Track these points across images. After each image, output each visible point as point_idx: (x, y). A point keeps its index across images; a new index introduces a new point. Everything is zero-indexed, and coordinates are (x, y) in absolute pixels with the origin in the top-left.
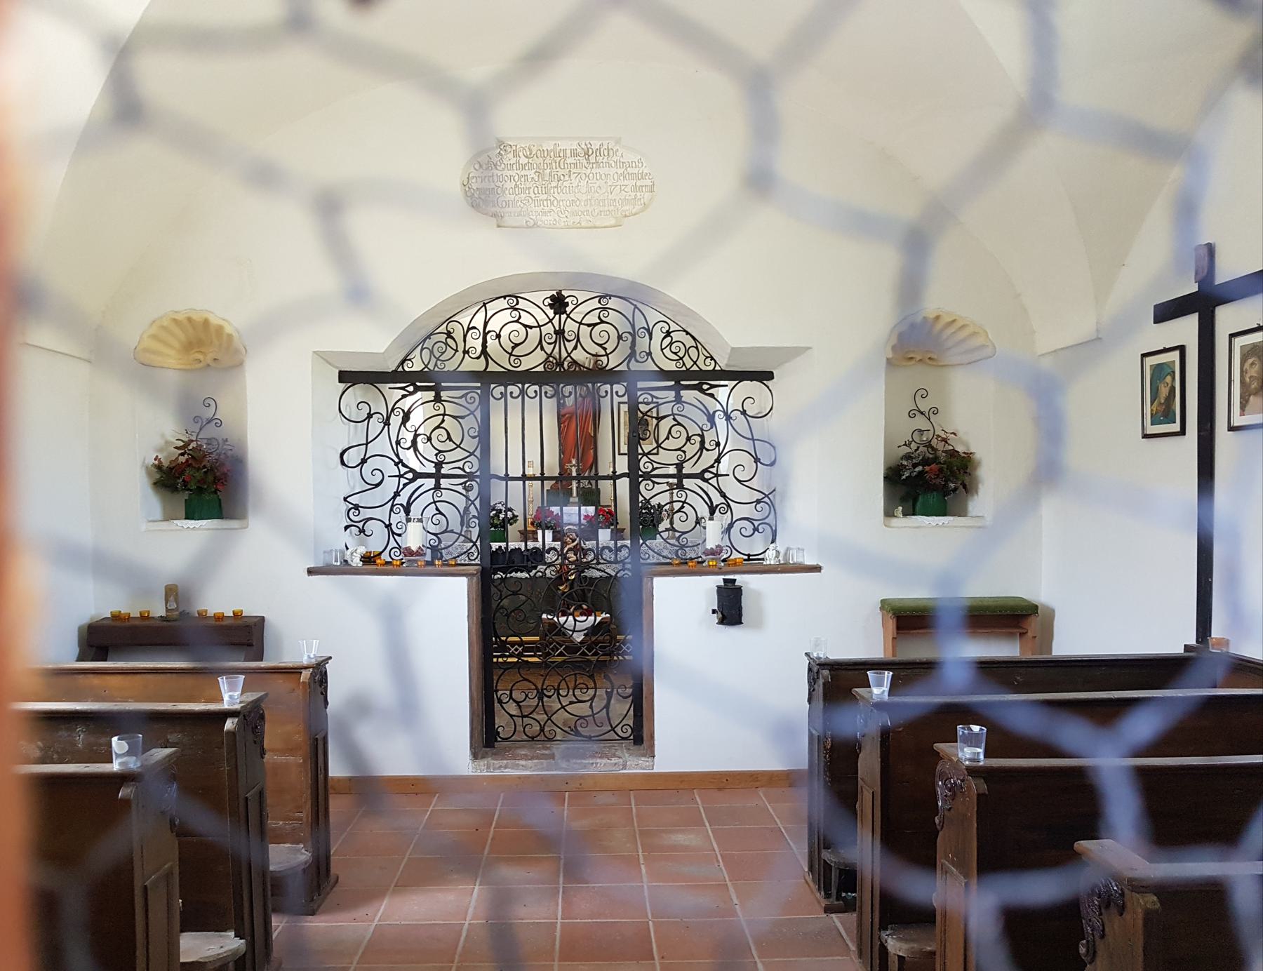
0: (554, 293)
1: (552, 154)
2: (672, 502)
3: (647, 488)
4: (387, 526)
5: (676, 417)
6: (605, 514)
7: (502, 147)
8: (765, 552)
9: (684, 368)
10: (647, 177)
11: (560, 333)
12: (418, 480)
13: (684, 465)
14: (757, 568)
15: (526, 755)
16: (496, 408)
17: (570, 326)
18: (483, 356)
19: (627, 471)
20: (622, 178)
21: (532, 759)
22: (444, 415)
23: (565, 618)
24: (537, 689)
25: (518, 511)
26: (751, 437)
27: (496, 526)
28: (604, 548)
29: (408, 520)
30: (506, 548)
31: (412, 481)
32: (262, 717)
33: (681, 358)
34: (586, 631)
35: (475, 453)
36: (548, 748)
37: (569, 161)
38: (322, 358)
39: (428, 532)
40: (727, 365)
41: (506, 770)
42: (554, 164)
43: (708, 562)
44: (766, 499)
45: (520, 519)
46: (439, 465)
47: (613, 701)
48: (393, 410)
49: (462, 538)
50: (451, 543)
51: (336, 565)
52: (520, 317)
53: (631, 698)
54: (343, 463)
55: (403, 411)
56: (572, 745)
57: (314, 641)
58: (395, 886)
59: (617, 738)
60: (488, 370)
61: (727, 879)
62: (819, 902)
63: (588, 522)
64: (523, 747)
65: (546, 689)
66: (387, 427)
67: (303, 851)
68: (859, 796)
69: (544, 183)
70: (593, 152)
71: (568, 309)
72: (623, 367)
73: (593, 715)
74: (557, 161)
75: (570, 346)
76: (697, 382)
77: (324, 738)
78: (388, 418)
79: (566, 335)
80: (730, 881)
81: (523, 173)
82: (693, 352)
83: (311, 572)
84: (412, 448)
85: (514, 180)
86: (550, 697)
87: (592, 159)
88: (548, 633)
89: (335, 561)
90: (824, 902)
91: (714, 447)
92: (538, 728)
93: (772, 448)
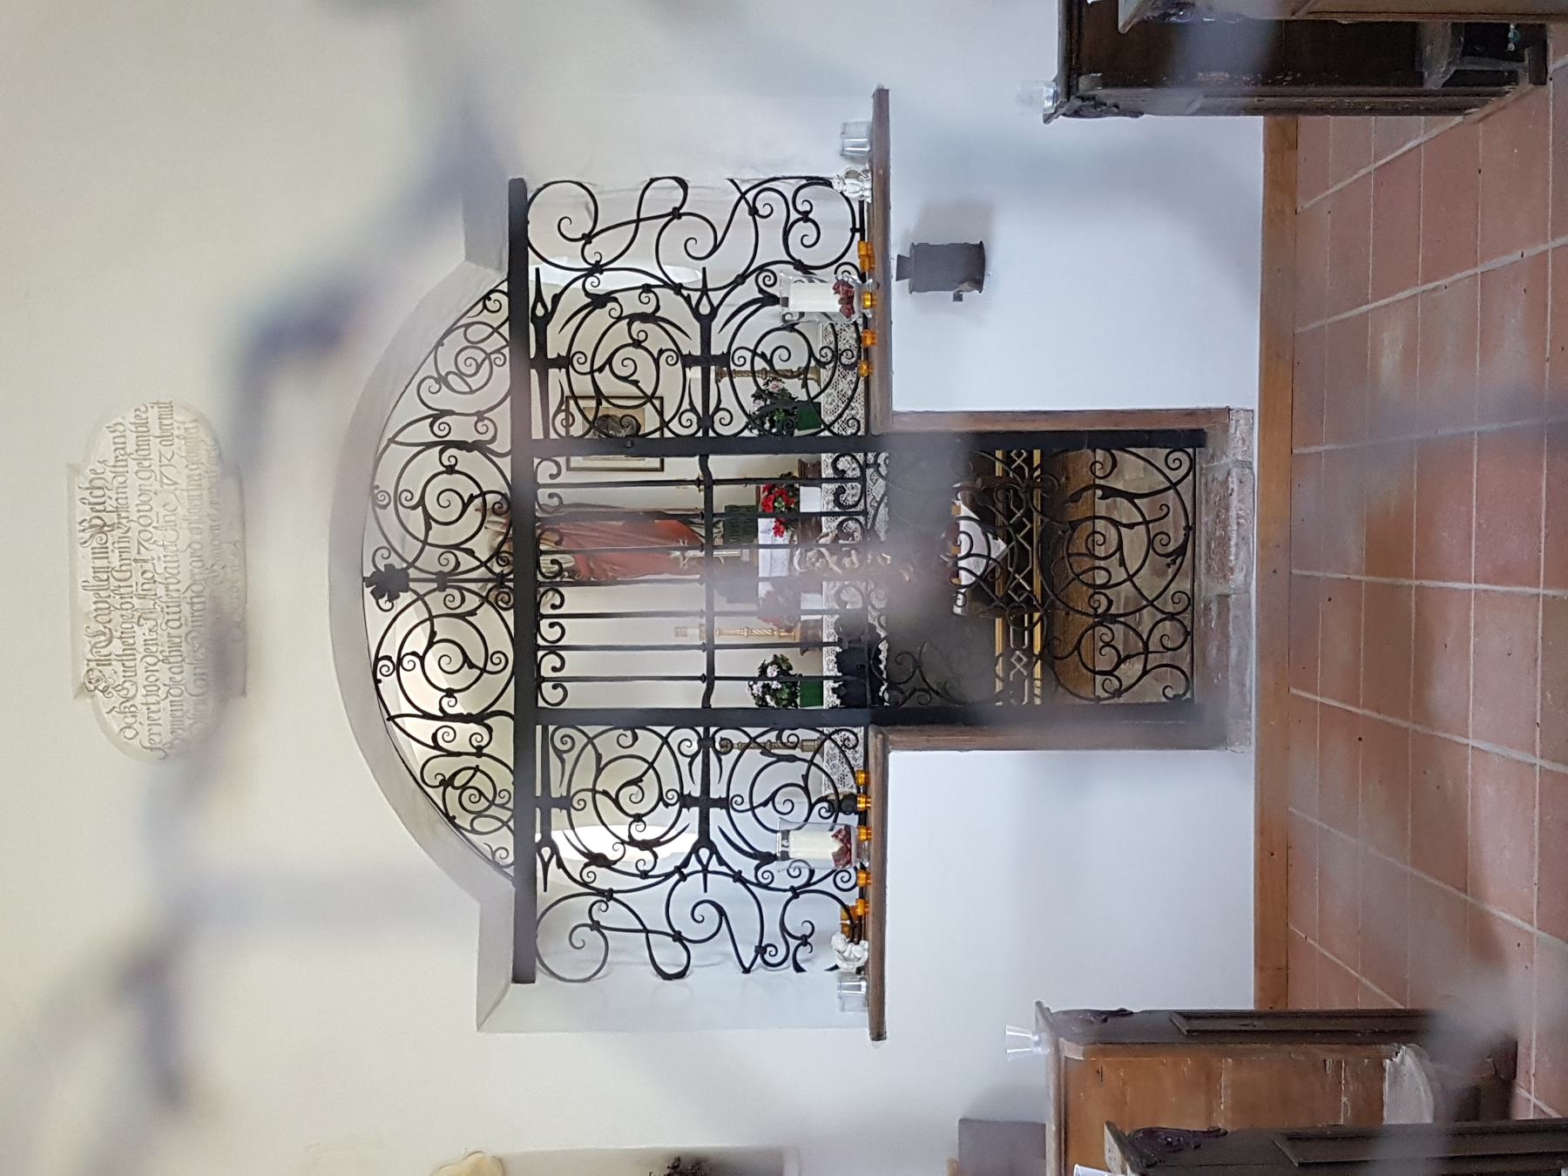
0: (368, 591)
1: (103, 594)
2: (753, 373)
3: (727, 421)
4: (796, 896)
5: (595, 367)
6: (772, 497)
7: (92, 687)
8: (847, 199)
9: (506, 351)
10: (144, 416)
11: (443, 581)
12: (712, 838)
13: (685, 352)
14: (877, 213)
15: (1219, 649)
16: (580, 697)
17: (431, 561)
18: (487, 722)
19: (697, 458)
20: (146, 463)
21: (1225, 635)
22: (594, 791)
23: (962, 573)
24: (1092, 627)
25: (768, 656)
26: (634, 225)
27: (793, 695)
28: (837, 502)
29: (785, 856)
30: (835, 679)
31: (714, 850)
32: (1151, 1133)
33: (488, 356)
34: (990, 536)
35: (664, 735)
36: (1207, 608)
37: (116, 563)
38: (490, 1013)
39: (806, 820)
40: (499, 269)
41: (1248, 683)
42: (122, 590)
43: (865, 308)
44: (750, 196)
45: (779, 652)
46: (685, 801)
47: (1120, 486)
48: (585, 884)
49: (817, 760)
50: (824, 776)
51: (867, 987)
52: (414, 654)
53: (1114, 451)
54: (681, 975)
55: (586, 865)
56: (1203, 561)
57: (1008, 1033)
58: (1466, 892)
59: (1190, 477)
60: (513, 713)
61: (1471, 272)
62: (1522, 96)
63: (787, 529)
64: (1204, 656)
65: (1096, 609)
66: (615, 895)
67: (1397, 1060)
68: (1327, 17)
69: (159, 609)
70: (98, 517)
71: (399, 565)
72: (505, 464)
73: (1146, 523)
74: (117, 583)
75: (467, 562)
76: (532, 327)
77: (1184, 1017)
78: (599, 892)
79: (447, 569)
80: (1476, 265)
81: (140, 647)
82: (477, 333)
83: (878, 1034)
84: (654, 849)
85: (155, 664)
86: (1110, 602)
87: (111, 518)
88: (993, 604)
89: (860, 990)
90: (1526, 85)
91: (651, 295)
92: (1167, 623)
93: (655, 184)
